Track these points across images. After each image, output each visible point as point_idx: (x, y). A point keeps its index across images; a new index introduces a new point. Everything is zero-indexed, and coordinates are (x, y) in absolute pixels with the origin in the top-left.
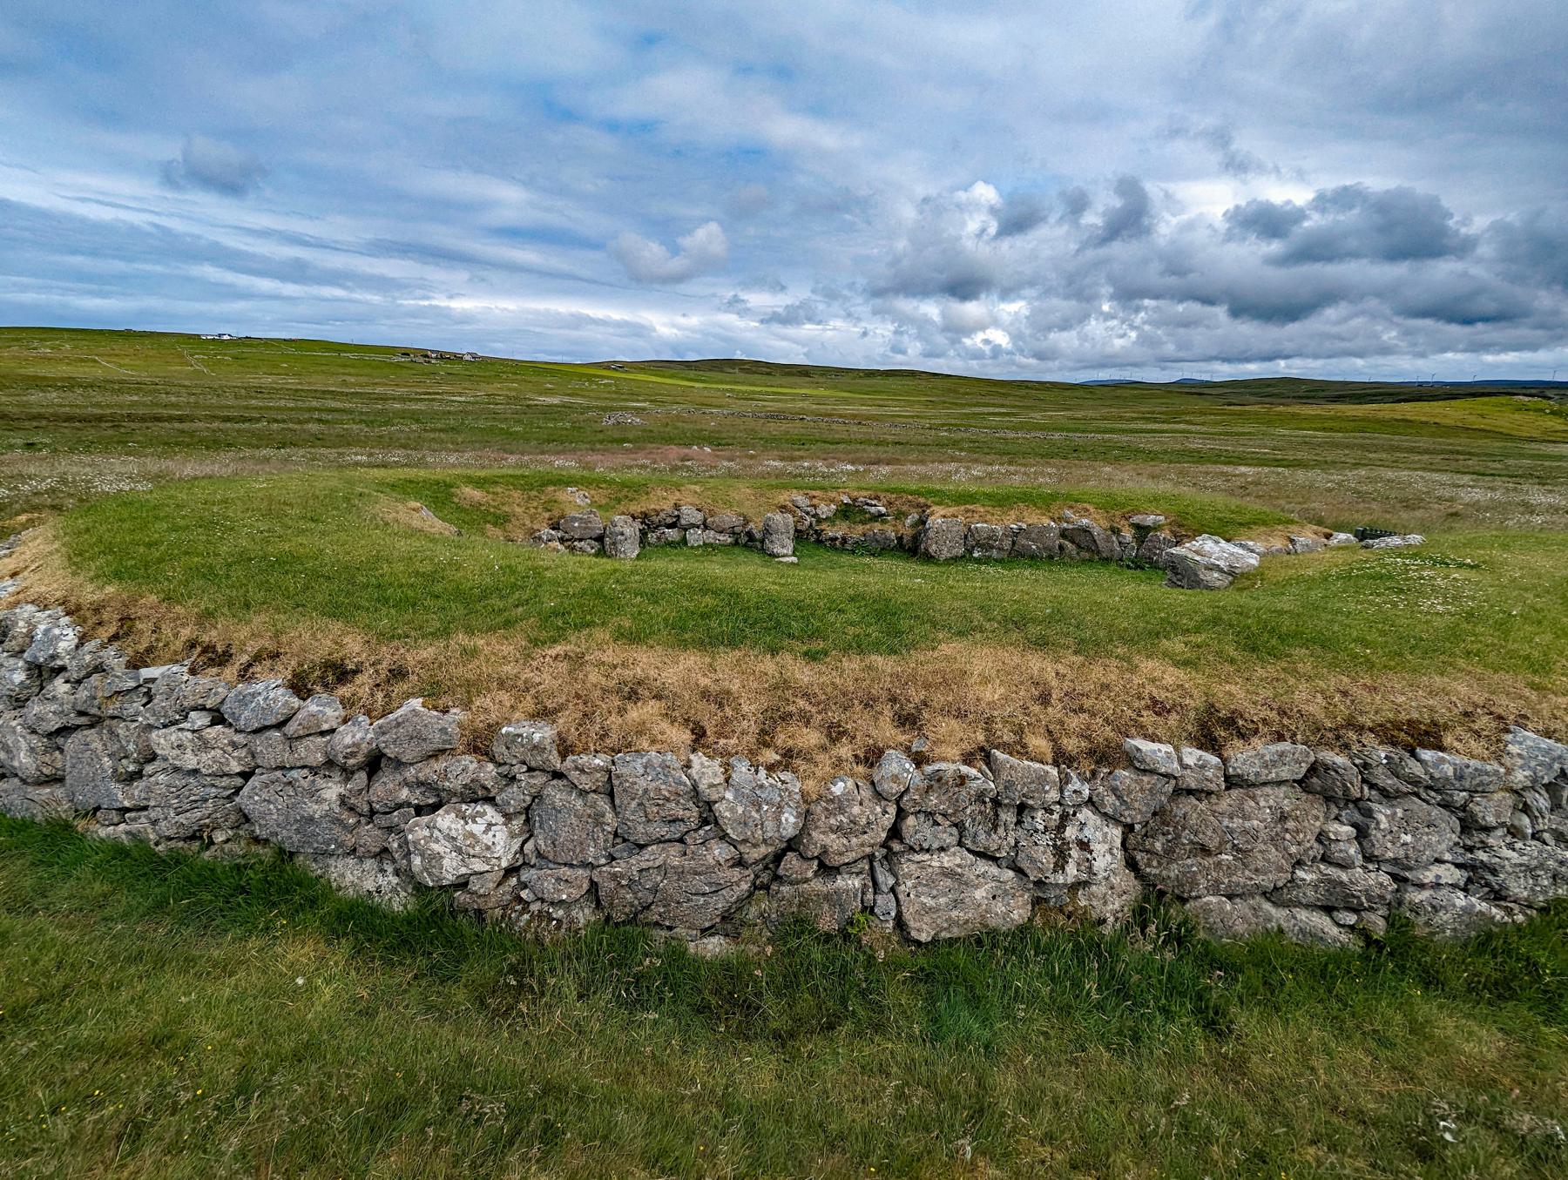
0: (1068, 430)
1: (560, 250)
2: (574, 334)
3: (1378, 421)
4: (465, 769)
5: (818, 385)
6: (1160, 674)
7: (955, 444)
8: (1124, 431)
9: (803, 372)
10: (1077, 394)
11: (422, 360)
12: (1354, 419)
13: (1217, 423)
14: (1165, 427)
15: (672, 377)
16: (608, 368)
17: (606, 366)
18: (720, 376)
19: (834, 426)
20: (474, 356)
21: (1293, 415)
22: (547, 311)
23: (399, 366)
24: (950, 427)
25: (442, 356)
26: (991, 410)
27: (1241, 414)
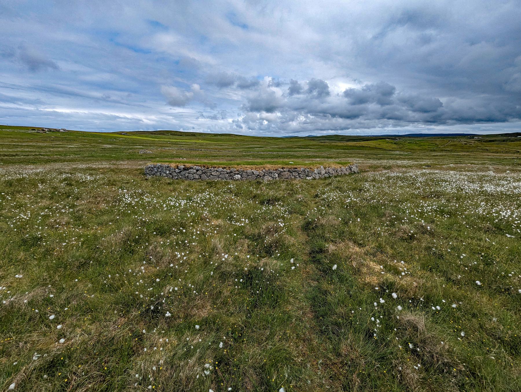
0: (278, 151)
1: (106, 93)
2: (112, 122)
3: (356, 146)
4: (237, 172)
5: (199, 139)
6: (279, 166)
7: (248, 156)
8: (293, 151)
9: (193, 135)
10: (280, 141)
11: (42, 132)
12: (351, 146)
13: (317, 148)
14: (304, 150)
15: (146, 137)
16: (121, 134)
17: (121, 133)
18: (164, 136)
19: (212, 152)
20: (64, 130)
21: (336, 145)
22: (101, 114)
23: (31, 134)
24: (245, 152)
25: (50, 130)
26: (255, 146)
27: (323, 145)
